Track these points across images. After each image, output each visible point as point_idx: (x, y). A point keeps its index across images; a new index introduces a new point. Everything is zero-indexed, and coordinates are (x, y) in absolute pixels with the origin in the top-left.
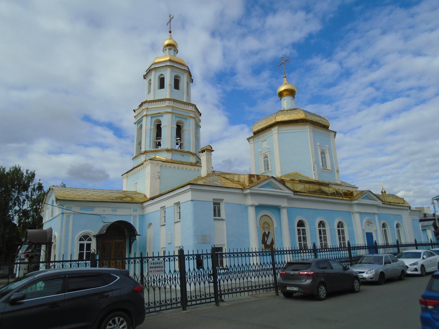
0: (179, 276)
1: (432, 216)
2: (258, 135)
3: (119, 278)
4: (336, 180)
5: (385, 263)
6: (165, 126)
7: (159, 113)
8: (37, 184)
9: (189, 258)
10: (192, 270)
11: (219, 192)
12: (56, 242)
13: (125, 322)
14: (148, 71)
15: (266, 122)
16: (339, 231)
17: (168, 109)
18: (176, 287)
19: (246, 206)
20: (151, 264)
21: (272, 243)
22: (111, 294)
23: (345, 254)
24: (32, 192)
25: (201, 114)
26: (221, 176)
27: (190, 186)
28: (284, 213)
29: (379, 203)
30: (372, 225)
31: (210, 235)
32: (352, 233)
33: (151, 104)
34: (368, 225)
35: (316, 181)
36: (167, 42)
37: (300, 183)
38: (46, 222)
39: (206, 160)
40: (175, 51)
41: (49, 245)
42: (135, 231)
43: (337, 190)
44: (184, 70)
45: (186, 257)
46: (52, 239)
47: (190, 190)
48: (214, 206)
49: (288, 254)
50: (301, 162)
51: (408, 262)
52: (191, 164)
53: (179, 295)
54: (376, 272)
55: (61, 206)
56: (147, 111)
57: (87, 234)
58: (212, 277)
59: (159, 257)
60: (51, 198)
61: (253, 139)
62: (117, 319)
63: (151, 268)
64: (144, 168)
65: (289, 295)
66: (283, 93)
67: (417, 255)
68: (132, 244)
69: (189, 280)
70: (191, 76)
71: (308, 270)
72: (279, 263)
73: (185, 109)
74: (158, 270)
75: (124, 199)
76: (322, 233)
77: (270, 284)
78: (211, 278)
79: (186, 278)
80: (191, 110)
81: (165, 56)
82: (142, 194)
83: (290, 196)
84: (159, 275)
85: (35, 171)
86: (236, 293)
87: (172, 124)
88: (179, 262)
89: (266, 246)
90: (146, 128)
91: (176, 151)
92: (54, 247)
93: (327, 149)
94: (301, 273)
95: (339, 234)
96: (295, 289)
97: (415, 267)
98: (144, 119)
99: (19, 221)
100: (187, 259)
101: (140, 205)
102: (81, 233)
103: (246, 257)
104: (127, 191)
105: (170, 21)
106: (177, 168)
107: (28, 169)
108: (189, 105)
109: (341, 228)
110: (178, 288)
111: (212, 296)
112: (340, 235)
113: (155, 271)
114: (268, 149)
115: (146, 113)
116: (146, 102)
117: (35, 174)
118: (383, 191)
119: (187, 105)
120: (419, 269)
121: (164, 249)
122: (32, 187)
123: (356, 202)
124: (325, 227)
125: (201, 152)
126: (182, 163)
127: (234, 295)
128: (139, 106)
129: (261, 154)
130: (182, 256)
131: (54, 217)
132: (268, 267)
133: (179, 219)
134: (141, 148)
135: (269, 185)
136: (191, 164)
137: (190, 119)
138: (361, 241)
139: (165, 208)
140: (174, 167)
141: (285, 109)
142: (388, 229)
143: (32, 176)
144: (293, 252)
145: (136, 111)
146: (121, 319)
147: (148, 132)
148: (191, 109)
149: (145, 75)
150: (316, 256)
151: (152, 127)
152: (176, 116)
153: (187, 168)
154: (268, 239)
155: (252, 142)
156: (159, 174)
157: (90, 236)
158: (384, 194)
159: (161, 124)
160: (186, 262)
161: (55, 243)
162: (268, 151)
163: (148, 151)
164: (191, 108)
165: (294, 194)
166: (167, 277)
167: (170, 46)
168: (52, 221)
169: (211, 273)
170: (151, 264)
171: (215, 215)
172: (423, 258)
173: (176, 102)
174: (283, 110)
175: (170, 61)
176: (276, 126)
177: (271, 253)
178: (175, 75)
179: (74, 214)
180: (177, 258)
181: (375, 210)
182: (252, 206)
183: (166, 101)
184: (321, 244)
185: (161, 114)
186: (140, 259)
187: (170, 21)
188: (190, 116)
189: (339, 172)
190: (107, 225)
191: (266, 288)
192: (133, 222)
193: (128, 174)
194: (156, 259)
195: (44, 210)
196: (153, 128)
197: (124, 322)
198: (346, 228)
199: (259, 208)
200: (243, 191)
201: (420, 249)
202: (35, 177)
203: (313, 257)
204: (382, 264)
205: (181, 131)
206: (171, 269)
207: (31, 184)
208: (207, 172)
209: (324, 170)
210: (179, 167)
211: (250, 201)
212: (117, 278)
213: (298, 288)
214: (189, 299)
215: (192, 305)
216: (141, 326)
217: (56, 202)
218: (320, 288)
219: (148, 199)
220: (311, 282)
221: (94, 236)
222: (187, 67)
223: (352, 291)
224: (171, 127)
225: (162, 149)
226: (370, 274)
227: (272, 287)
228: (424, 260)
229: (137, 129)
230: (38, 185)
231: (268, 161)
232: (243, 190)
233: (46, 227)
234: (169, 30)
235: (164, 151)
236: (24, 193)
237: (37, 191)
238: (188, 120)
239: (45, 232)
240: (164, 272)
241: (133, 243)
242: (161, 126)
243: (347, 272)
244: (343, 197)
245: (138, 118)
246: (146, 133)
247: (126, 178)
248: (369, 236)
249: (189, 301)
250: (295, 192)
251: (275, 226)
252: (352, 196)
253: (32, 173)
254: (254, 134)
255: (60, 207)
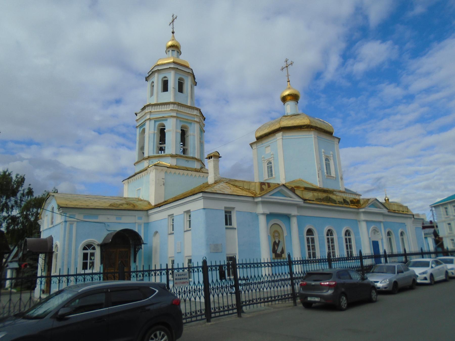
0: (203, 287)
1: (429, 223)
2: (261, 141)
3: (157, 291)
4: (340, 187)
5: (398, 273)
6: (169, 131)
7: (163, 117)
8: (27, 189)
9: (212, 269)
10: (215, 281)
11: (231, 200)
12: (57, 251)
13: (166, 336)
14: (151, 73)
15: (269, 127)
16: (328, 239)
17: (172, 113)
18: (195, 299)
19: (257, 214)
20: (176, 275)
21: (283, 252)
22: (151, 307)
23: (356, 264)
24: (21, 197)
25: (205, 118)
26: (230, 183)
27: (202, 194)
28: (294, 222)
29: (384, 211)
30: (378, 233)
31: (222, 244)
32: (358, 242)
33: (164, 107)
34: (374, 234)
35: (321, 189)
36: (170, 43)
37: (305, 190)
38: (43, 230)
39: (213, 166)
40: (178, 52)
41: (49, 254)
42: (141, 240)
43: (344, 198)
44: (188, 72)
45: (209, 268)
46: (53, 248)
47: (202, 198)
48: (225, 214)
49: (297, 264)
50: (306, 169)
51: (418, 271)
52: (196, 170)
53: (203, 307)
54: (390, 281)
55: (64, 213)
56: (150, 115)
57: (90, 243)
58: (234, 288)
59: (183, 269)
60: (52, 204)
61: (256, 144)
62: (158, 333)
63: (176, 279)
64: (147, 174)
65: (308, 305)
66: (287, 97)
67: (426, 264)
68: (137, 253)
69: (212, 291)
70: (194, 78)
71: (330, 280)
72: (296, 273)
73: (190, 113)
74: (183, 282)
75: (121, 206)
76: (331, 241)
77: (288, 295)
78: (233, 289)
79: (210, 290)
80: (196, 115)
81: (169, 58)
82: (145, 201)
83: (300, 204)
84: (184, 287)
85: (24, 175)
86: (257, 303)
87: (176, 128)
88: (203, 273)
89: (278, 256)
90: (149, 132)
91: (181, 156)
92: (55, 256)
93: (332, 156)
94: (322, 283)
95: (328, 242)
96: (317, 299)
97: (425, 275)
98: (147, 123)
99: (7, 228)
100: (210, 270)
101: (145, 212)
102: (84, 242)
103: (265, 268)
104: (129, 198)
105: (173, 21)
106: (182, 174)
107: (18, 173)
108: (193, 109)
109: (330, 236)
110: (203, 300)
111: (235, 307)
112: (309, 243)
113: (180, 283)
114: (272, 155)
115: (149, 116)
116: (148, 106)
117: (25, 178)
118: (387, 199)
119: (191, 109)
120: (428, 278)
121: (173, 259)
122: (22, 192)
123: (363, 210)
124: (313, 235)
125: (208, 158)
126: (187, 169)
127: (255, 305)
128: (142, 109)
129: (264, 160)
130: (205, 268)
131: (54, 225)
132: (286, 277)
133: (189, 228)
134: (143, 153)
135: (280, 193)
136: (196, 170)
137: (195, 124)
138: (367, 250)
139: (173, 216)
140: (175, 173)
141: (289, 114)
142: (393, 237)
143: (21, 181)
144: (303, 262)
145: (138, 114)
146: (162, 333)
147: (152, 136)
148: (196, 113)
149: (148, 77)
150: (330, 266)
151: (156, 132)
152: (180, 121)
153: (192, 175)
154: (278, 249)
155: (256, 147)
156: (164, 180)
157: (94, 245)
158: (387, 201)
159: (165, 128)
160: (210, 273)
161: (57, 252)
162: (272, 157)
163: (151, 156)
164: (195, 112)
165: (304, 202)
166: (192, 288)
167: (173, 47)
168: (52, 229)
169: (233, 284)
170: (176, 275)
171: (226, 224)
172: (432, 267)
173: (181, 106)
174: (286, 115)
175: (174, 63)
176: (281, 132)
177: (288, 263)
178: (178, 78)
179: (77, 222)
180: (201, 269)
181: (381, 219)
182: (263, 214)
183: (171, 105)
184: (348, 252)
185: (165, 119)
186: (166, 271)
187: (173, 21)
188: (195, 121)
189: (343, 179)
190: (111, 234)
191: (283, 298)
192: (138, 230)
193: (130, 180)
194: (181, 271)
195: (42, 217)
196: (157, 133)
197: (165, 336)
198: (352, 237)
199: (269, 216)
200: (254, 199)
201: (426, 258)
202: (25, 182)
203: (328, 267)
204: (395, 273)
205: (185, 136)
206: (195, 281)
207: (20, 189)
208: (215, 178)
209: (329, 178)
210: (184, 173)
211: (260, 209)
212: (155, 291)
213: (319, 298)
214: (212, 311)
215: (215, 317)
216: (180, 339)
217: (58, 209)
218: (341, 299)
219: (153, 206)
220: (333, 293)
221: (98, 245)
222: (192, 69)
223: (370, 301)
224: (176, 132)
225: (166, 155)
226: (384, 283)
227: (290, 298)
228: (433, 269)
229: (139, 134)
230: (28, 191)
231: (271, 167)
232: (254, 198)
233: (44, 236)
234: (172, 31)
235: (169, 156)
236: (13, 199)
237: (27, 197)
238: (193, 124)
239: (45, 241)
240: (189, 283)
241: (139, 252)
242: (165, 130)
243: (365, 282)
244: (350, 205)
245: (143, 120)
246: (149, 137)
247: (127, 184)
248: (375, 245)
249: (213, 313)
250: (305, 200)
251: (285, 234)
252: (359, 204)
253: (22, 177)
254: (257, 140)
255: (63, 214)
